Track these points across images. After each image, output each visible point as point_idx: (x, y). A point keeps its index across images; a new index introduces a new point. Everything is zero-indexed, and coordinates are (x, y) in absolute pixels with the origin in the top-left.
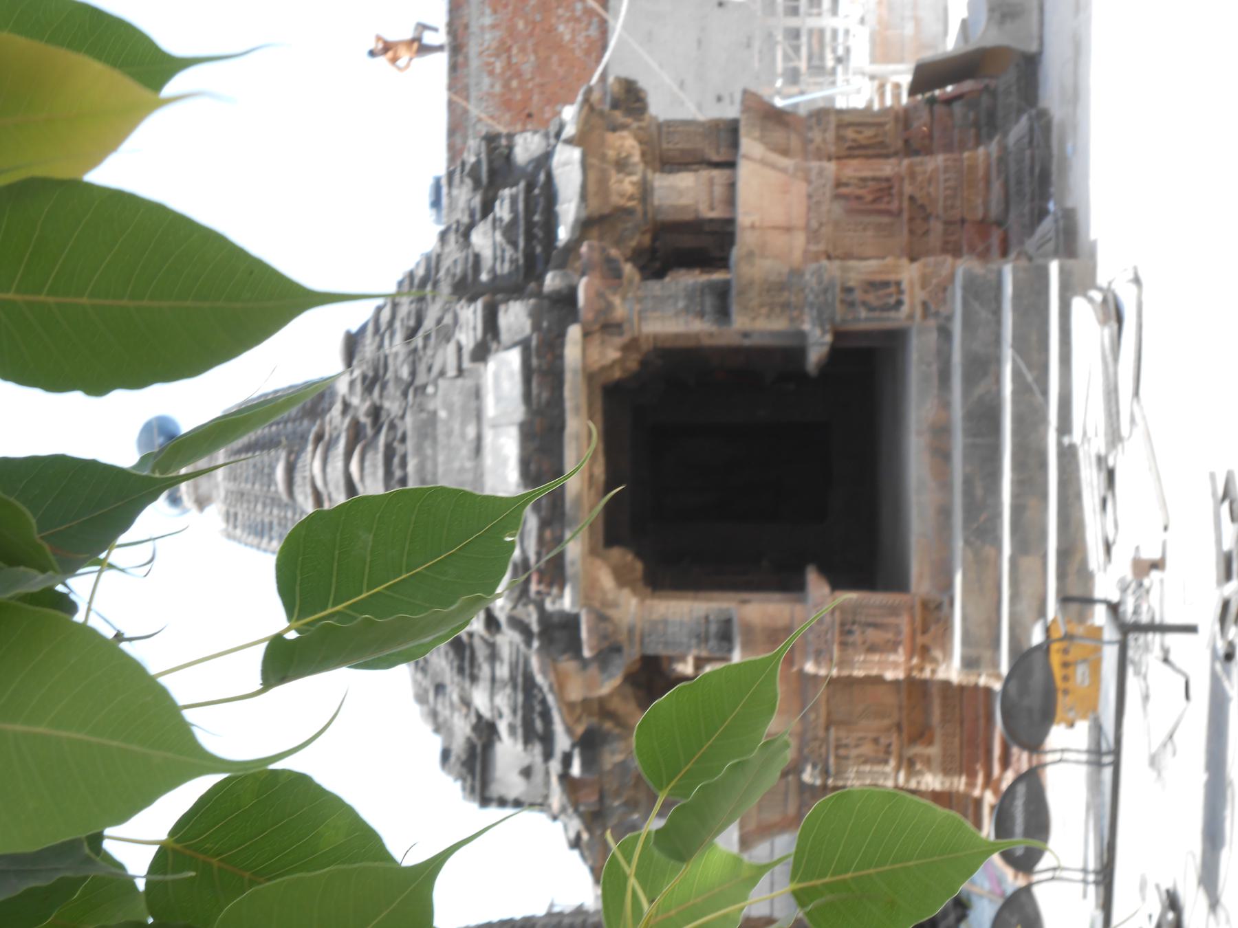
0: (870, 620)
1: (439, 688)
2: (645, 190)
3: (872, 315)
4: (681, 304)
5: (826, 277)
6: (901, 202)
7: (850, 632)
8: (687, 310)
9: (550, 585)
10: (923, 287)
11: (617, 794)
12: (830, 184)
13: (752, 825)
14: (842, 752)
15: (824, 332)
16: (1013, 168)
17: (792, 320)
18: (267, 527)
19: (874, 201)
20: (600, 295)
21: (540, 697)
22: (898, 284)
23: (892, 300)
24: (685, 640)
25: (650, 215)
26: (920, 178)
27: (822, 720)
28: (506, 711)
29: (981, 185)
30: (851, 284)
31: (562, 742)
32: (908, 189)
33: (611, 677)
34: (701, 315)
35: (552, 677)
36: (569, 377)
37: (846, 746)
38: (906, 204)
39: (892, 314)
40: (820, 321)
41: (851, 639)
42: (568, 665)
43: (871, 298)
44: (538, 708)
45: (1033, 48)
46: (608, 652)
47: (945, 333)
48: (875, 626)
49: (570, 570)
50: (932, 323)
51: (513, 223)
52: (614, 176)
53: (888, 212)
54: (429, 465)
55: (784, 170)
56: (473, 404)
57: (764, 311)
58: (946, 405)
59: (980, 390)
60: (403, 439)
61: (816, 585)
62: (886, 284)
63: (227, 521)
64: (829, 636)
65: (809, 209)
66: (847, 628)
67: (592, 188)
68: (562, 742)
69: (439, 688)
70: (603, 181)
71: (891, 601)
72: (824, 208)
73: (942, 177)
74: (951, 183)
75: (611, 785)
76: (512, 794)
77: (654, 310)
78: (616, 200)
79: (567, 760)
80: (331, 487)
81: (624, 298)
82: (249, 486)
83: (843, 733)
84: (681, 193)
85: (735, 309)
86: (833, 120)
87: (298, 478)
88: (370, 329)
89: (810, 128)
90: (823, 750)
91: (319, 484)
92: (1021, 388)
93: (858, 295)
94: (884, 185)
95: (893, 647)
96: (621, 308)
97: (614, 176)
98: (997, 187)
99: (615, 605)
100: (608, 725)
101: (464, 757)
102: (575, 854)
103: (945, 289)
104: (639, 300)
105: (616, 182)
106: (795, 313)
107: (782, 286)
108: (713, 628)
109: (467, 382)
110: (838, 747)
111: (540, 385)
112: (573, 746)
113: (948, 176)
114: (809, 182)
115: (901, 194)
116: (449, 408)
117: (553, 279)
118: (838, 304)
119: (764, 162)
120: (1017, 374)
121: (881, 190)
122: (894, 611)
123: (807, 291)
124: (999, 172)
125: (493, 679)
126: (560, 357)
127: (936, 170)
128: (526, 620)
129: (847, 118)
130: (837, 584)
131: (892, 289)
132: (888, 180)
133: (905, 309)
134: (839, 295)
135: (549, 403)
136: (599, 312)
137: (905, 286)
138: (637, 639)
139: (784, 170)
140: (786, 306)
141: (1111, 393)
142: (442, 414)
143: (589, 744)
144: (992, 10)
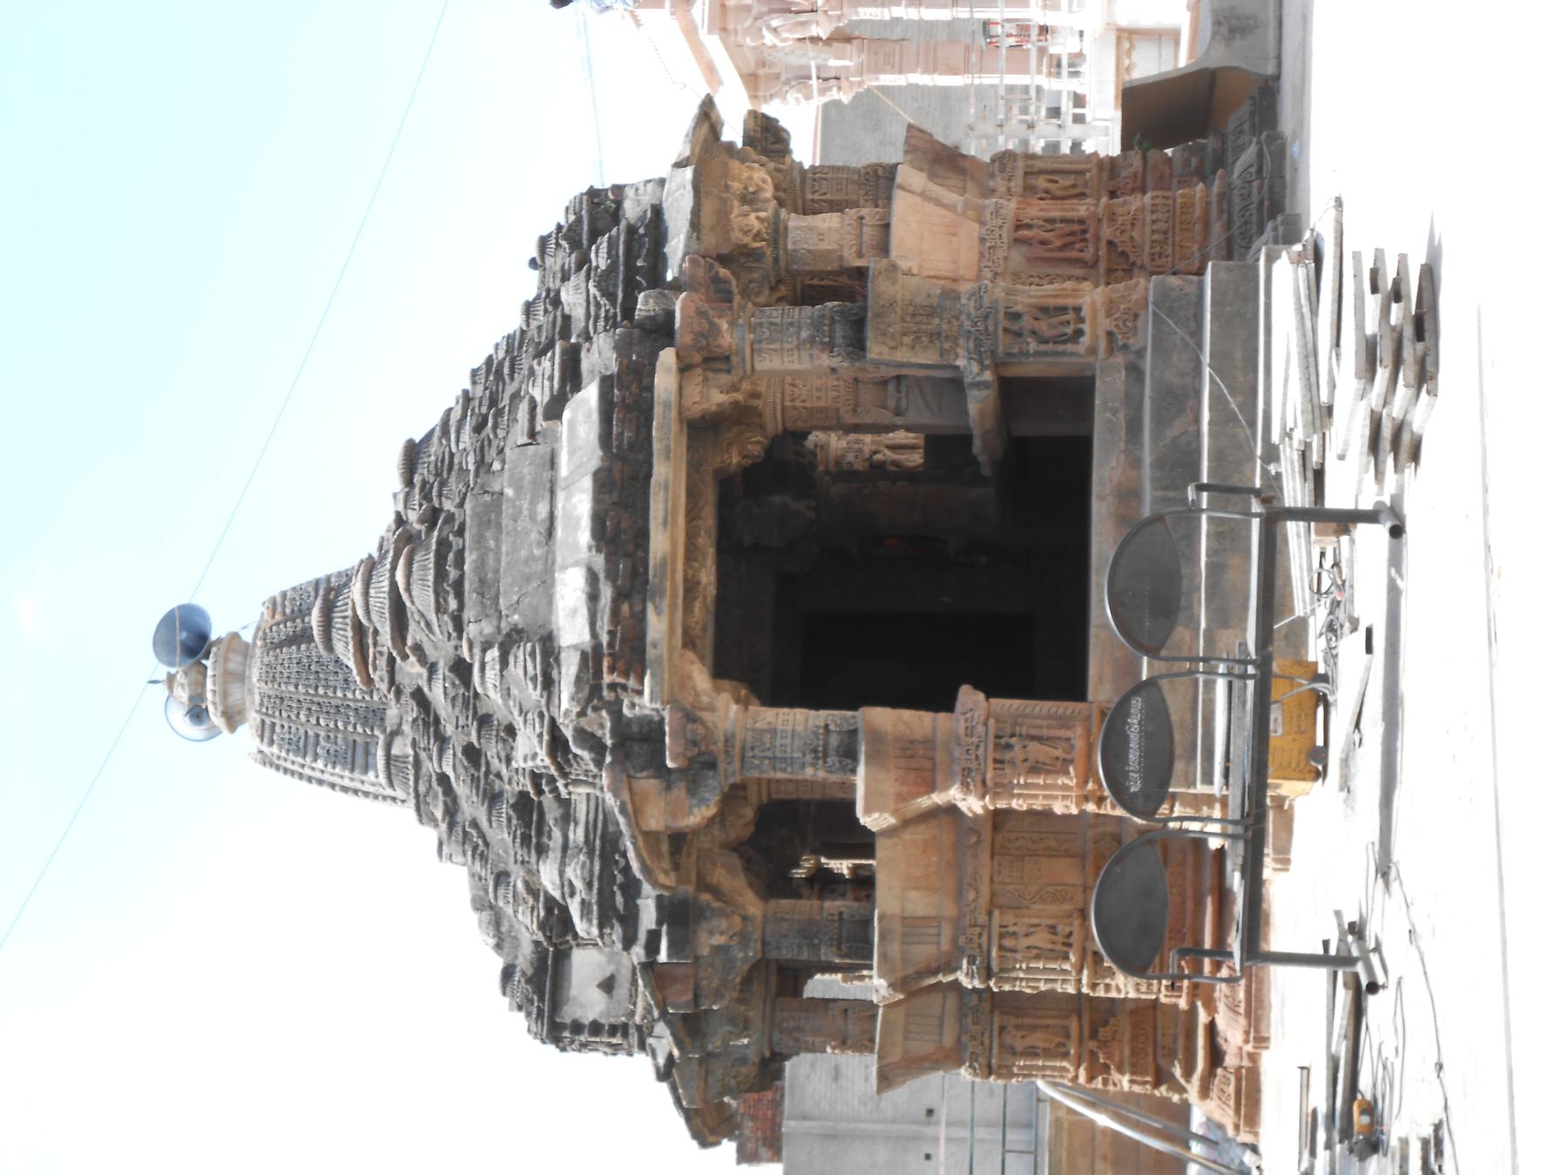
0: (1034, 732)
1: (501, 877)
2: (777, 232)
3: (1043, 347)
4: (804, 334)
5: (986, 301)
6: (1097, 249)
7: (1009, 747)
8: (812, 341)
9: (626, 675)
10: (1109, 315)
11: (718, 995)
12: (1009, 225)
13: (895, 1056)
14: (1007, 943)
15: (983, 368)
16: (1237, 204)
17: (942, 353)
18: (311, 741)
19: (1064, 247)
20: (701, 313)
21: (622, 862)
22: (1078, 310)
23: (1069, 330)
24: (797, 755)
25: (782, 263)
26: (1120, 220)
27: (984, 900)
28: (579, 885)
29: (1198, 227)
30: (1018, 308)
31: (648, 915)
32: (1106, 232)
33: (703, 802)
34: (830, 347)
35: (626, 796)
36: (658, 411)
37: (1014, 934)
38: (1103, 251)
39: (1069, 347)
40: (978, 355)
41: (1008, 756)
42: (648, 784)
43: (1043, 326)
44: (619, 878)
45: (1270, 70)
46: (700, 765)
47: (1135, 371)
48: (1040, 739)
49: (651, 653)
50: (1119, 359)
51: (612, 269)
52: (737, 208)
53: (1081, 262)
54: (491, 562)
55: (951, 208)
56: (547, 475)
57: (907, 340)
58: (1136, 463)
59: (1174, 430)
60: (460, 532)
61: (969, 698)
62: (1063, 310)
63: (262, 737)
64: (981, 752)
65: (982, 255)
66: (1003, 741)
67: (707, 219)
68: (648, 915)
69: (501, 877)
70: (723, 214)
71: (1061, 711)
72: (1001, 254)
73: (1149, 219)
74: (1160, 226)
75: (709, 979)
76: (588, 1017)
77: (771, 340)
78: (737, 236)
79: (653, 938)
80: (374, 617)
81: (732, 324)
82: (292, 688)
83: (1009, 918)
84: (821, 236)
85: (870, 333)
86: (1020, 164)
87: (337, 621)
88: (437, 433)
89: (992, 176)
90: (984, 940)
91: (360, 612)
92: (1222, 417)
93: (1026, 323)
94: (1076, 227)
95: (1061, 766)
96: (728, 337)
97: (737, 208)
98: (1217, 227)
99: (711, 708)
100: (705, 897)
101: (530, 972)
102: (664, 1087)
103: (1136, 316)
104: (752, 328)
105: (739, 215)
106: (946, 346)
107: (931, 312)
108: (834, 741)
109: (542, 449)
110: (1002, 936)
111: (621, 421)
112: (660, 922)
113: (1154, 217)
114: (982, 223)
115: (1097, 238)
116: (518, 489)
117: (646, 302)
118: (1000, 333)
119: (923, 195)
120: (1217, 398)
121: (1073, 234)
122: (1065, 722)
123: (963, 317)
124: (1221, 212)
125: (565, 847)
126: (650, 388)
127: (1142, 209)
128: (599, 733)
129: (1039, 165)
130: (992, 690)
131: (1070, 316)
132: (1081, 221)
133: (1085, 340)
134: (1003, 322)
135: (631, 446)
136: (699, 335)
137: (1085, 312)
138: (737, 751)
139: (951, 208)
140: (935, 336)
141: (1310, 355)
142: (509, 492)
143: (677, 914)
144: (1217, 23)
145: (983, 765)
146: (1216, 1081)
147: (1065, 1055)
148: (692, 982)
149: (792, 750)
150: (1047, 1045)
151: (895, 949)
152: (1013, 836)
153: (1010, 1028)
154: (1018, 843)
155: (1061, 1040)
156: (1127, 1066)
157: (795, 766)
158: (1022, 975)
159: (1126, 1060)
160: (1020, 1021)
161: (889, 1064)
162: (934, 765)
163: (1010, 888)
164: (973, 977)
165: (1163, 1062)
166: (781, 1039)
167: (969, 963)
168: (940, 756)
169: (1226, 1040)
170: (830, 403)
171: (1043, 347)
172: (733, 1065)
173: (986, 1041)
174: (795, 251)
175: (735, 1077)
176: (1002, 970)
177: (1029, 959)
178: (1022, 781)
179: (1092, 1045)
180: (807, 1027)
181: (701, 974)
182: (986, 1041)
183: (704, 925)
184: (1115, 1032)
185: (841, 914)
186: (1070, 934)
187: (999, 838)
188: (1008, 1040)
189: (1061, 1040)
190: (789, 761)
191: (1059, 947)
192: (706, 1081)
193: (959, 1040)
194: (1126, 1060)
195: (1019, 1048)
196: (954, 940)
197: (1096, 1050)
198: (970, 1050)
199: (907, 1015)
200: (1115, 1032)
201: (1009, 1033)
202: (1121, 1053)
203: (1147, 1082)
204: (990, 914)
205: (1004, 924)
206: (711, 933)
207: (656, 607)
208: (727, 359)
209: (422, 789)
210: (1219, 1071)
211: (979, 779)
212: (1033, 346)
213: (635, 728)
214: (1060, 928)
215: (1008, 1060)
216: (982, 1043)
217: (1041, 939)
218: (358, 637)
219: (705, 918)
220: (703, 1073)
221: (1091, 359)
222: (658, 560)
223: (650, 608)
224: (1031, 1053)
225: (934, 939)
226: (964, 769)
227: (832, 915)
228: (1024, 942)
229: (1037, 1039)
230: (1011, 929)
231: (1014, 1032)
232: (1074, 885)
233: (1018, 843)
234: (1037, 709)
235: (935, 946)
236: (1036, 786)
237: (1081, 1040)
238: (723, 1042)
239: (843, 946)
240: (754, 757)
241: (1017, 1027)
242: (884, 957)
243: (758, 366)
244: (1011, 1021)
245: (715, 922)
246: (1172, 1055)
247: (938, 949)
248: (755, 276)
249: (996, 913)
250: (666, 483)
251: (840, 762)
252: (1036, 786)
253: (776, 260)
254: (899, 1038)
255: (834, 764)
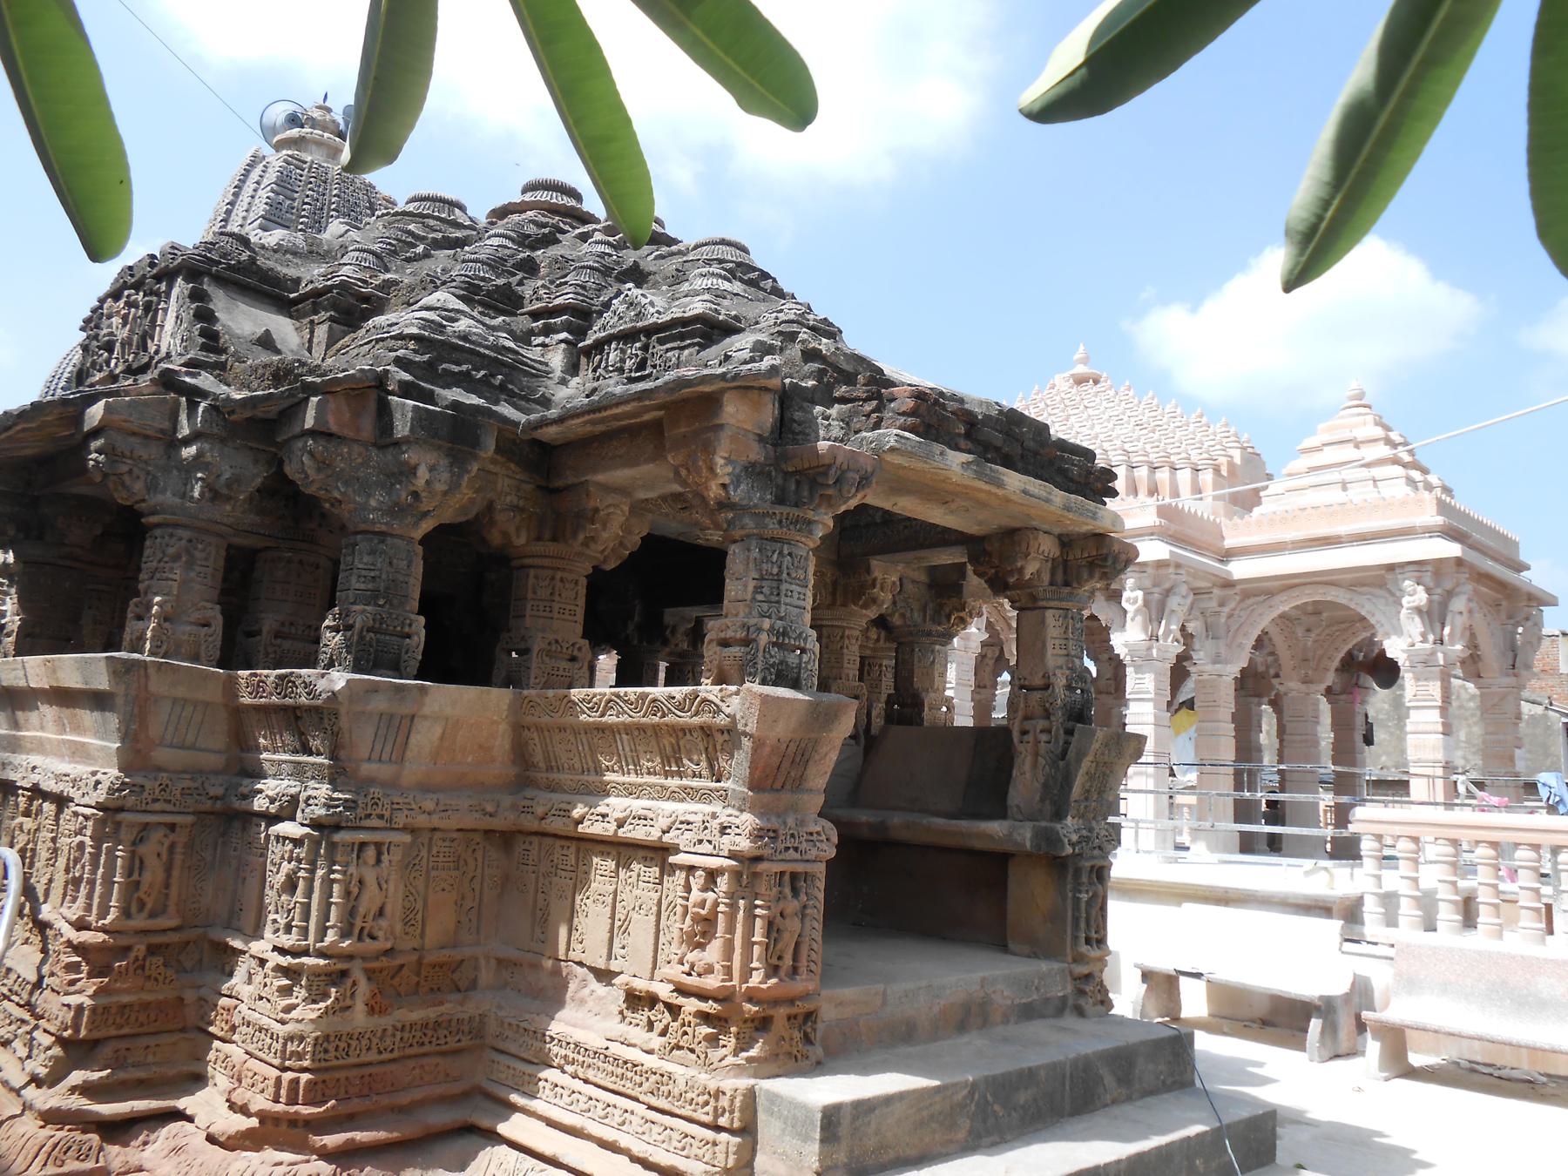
14: (370, 853)
27: (421, 821)
37: (379, 861)
108: (792, 659)
110: (378, 846)
145: (780, 857)
146: (78, 1136)
147: (126, 913)
148: (351, 434)
149: (786, 604)
150: (144, 887)
151: (379, 704)
152: (479, 854)
153: (172, 837)
154: (471, 862)
155: (149, 906)
156: (104, 1001)
157: (765, 606)
158: (320, 873)
159: (115, 999)
160: (179, 850)
161: (147, 676)
162: (777, 790)
163: (424, 853)
164: (329, 807)
165: (107, 1051)
166: (181, 539)
167: (346, 800)
168: (786, 797)
169: (145, 1143)
170: (846, 671)
171: (1083, 906)
172: (148, 473)
173: (157, 806)
174: (933, 651)
175: (130, 471)
176: (332, 846)
177: (346, 885)
178: (758, 911)
179: (140, 949)
180: (193, 574)
181: (356, 448)
182: (157, 806)
183: (444, 462)
184: (156, 980)
185: (408, 636)
186: (373, 938)
187: (478, 838)
188: (156, 836)
189: (149, 906)
190: (774, 598)
191: (358, 923)
192: (134, 434)
193: (159, 769)
194: (115, 999)
195: (143, 849)
196: (371, 781)
197: (132, 955)
198: (148, 785)
199: (207, 704)
200: (156, 980)
201: (165, 836)
202: (127, 991)
203: (77, 1029)
204: (404, 829)
205: (392, 848)
206: (432, 469)
207: (969, 463)
208: (1067, 584)
209: (432, 222)
210: (94, 1138)
211: (767, 852)
212: (1084, 897)
213: (798, 415)
214: (383, 923)
215: (127, 835)
216: (156, 800)
217: (369, 900)
218: (562, 210)
219: (451, 465)
220: (149, 432)
221: (1070, 959)
222: (1005, 478)
223: (970, 457)
224: (135, 865)
225: (375, 755)
226: (774, 831)
227: (410, 625)
228: (370, 876)
229: (153, 874)
230: (385, 857)
231: (167, 843)
232: (422, 935)
233: (471, 862)
234: (816, 925)
235: (366, 756)
236: (749, 932)
237: (145, 932)
238: (208, 464)
239: (372, 635)
240: (781, 553)
241: (172, 846)
242: (374, 689)
243: (1049, 613)
244: (181, 838)
245: (445, 476)
246: (117, 1064)
247: (362, 760)
248: (916, 615)
249: (407, 838)
250: (1047, 501)
251: (772, 666)
252: (749, 932)
253: (929, 634)
254: (180, 692)
255: (772, 657)
